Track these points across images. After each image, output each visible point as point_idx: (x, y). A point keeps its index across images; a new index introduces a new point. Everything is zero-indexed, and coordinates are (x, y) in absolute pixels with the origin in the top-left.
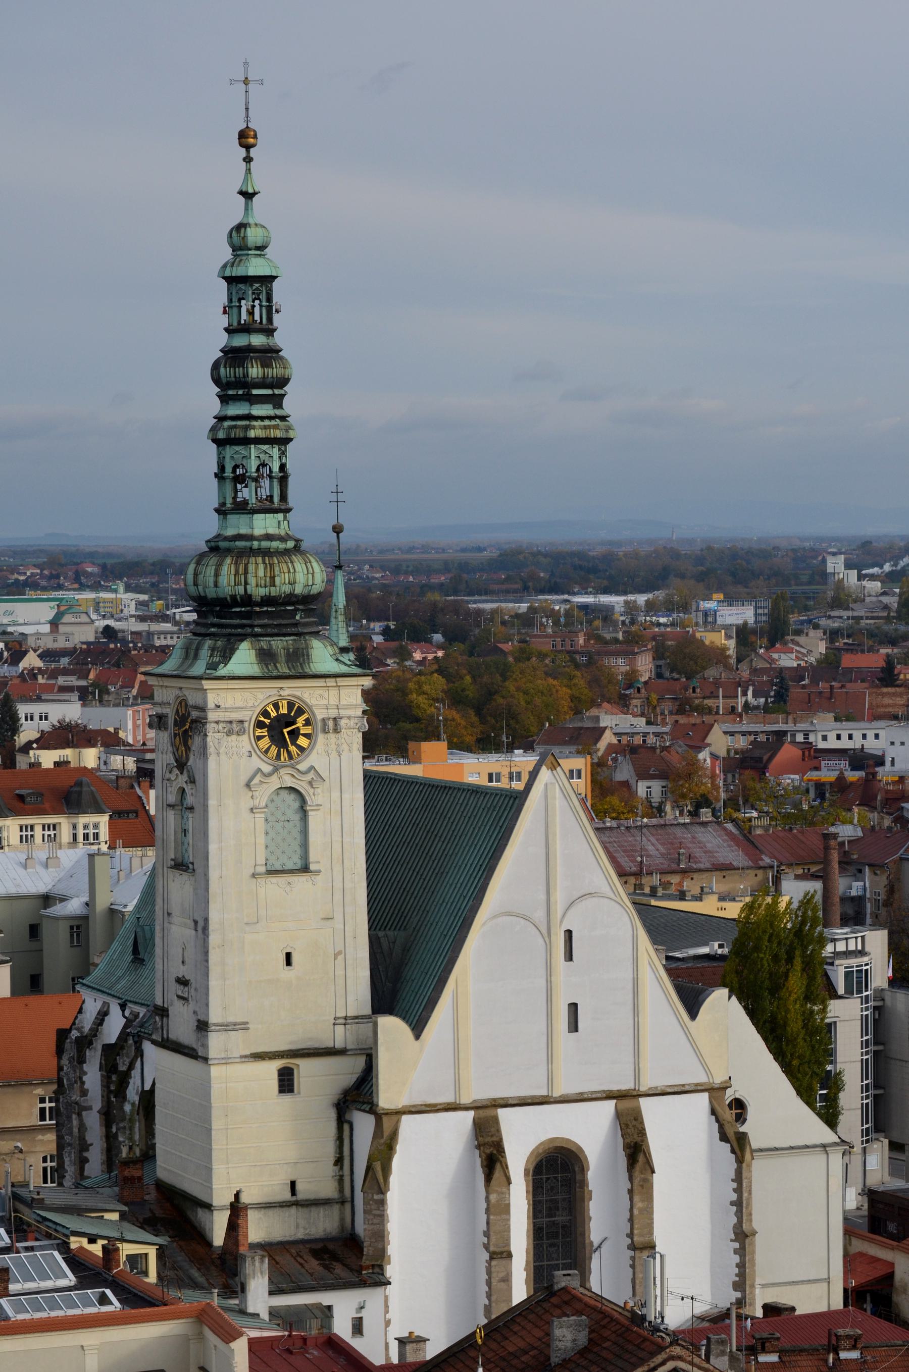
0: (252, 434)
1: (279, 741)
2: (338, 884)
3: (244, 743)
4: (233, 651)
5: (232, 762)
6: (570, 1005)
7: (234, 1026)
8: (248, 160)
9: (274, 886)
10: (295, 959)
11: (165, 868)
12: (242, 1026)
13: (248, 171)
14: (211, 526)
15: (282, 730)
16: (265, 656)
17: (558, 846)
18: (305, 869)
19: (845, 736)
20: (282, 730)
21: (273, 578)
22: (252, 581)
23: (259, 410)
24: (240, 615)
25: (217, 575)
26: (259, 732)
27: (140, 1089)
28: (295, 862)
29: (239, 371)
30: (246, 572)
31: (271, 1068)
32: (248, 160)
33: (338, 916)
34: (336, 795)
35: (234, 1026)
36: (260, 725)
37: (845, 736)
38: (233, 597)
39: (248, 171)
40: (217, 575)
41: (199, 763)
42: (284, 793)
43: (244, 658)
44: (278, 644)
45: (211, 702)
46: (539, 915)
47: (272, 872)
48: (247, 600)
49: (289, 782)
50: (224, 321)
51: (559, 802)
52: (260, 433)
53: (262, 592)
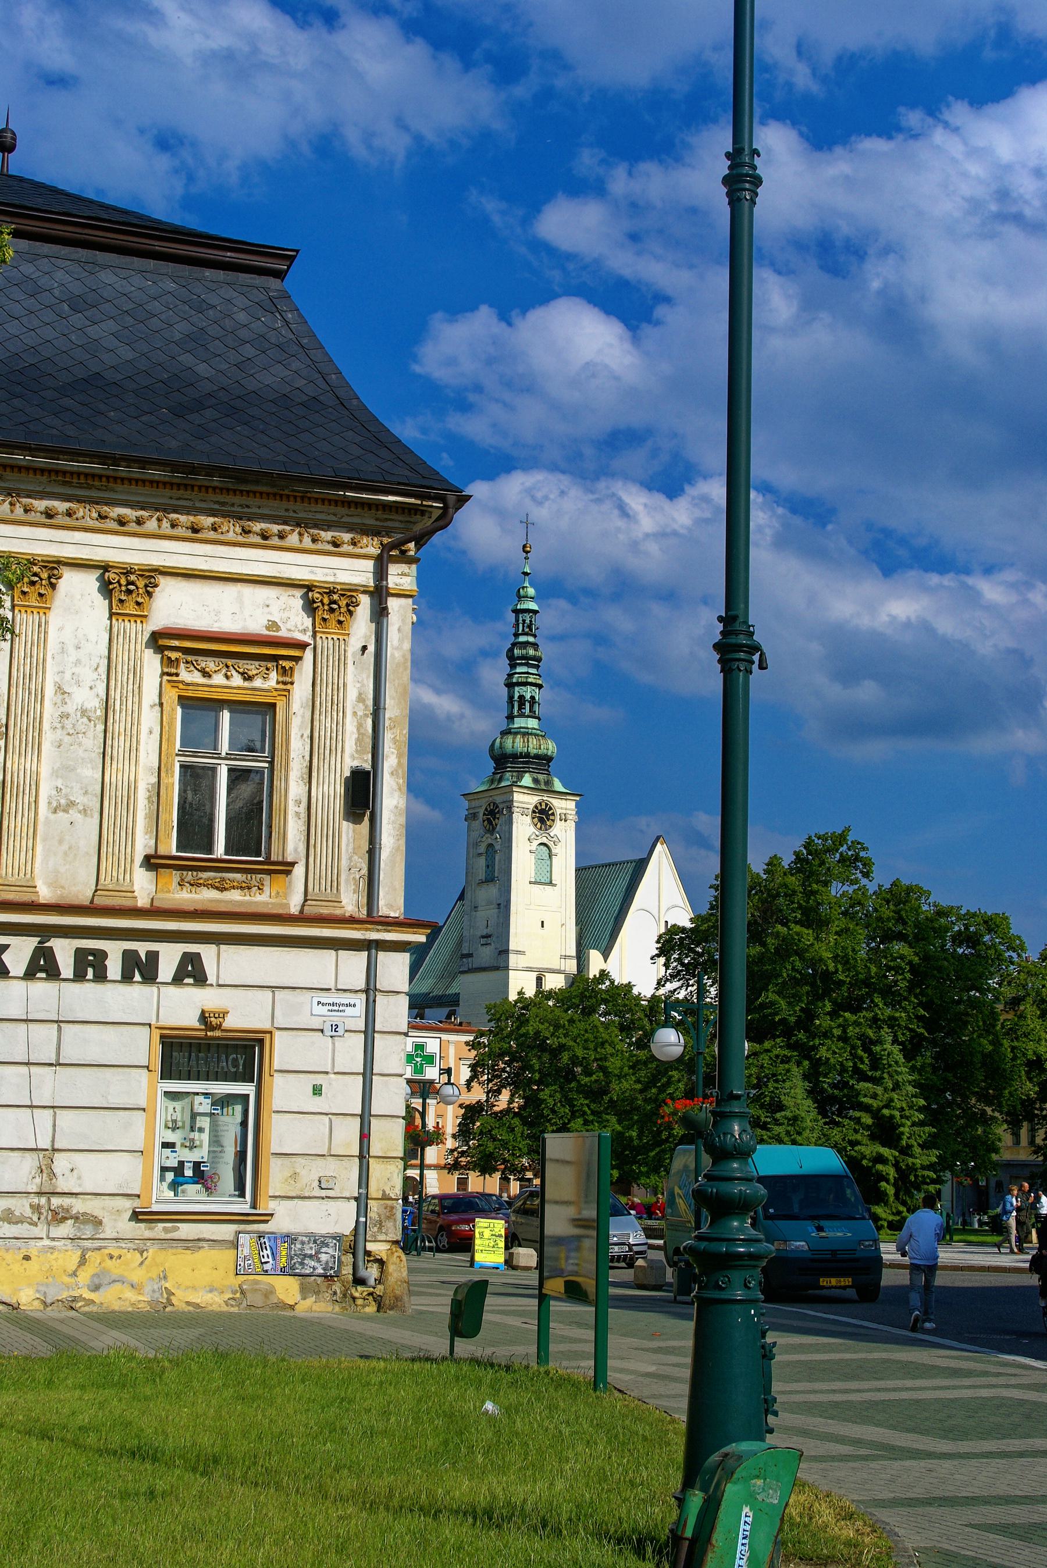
0: (530, 680)
1: (541, 820)
3: (528, 819)
4: (522, 777)
5: (523, 828)
6: (766, 668)
7: (518, 952)
11: (563, 840)
15: (543, 816)
16: (536, 781)
18: (550, 883)
19: (744, 1541)
20: (543, 816)
22: (531, 745)
23: (531, 671)
28: (548, 881)
29: (524, 652)
31: (534, 975)
35: (518, 952)
37: (744, 1541)
41: (505, 828)
43: (527, 780)
44: (541, 777)
45: (515, 799)
46: (655, 913)
47: (535, 883)
48: (527, 755)
49: (545, 840)
51: (664, 860)
52: (534, 681)
53: (535, 751)
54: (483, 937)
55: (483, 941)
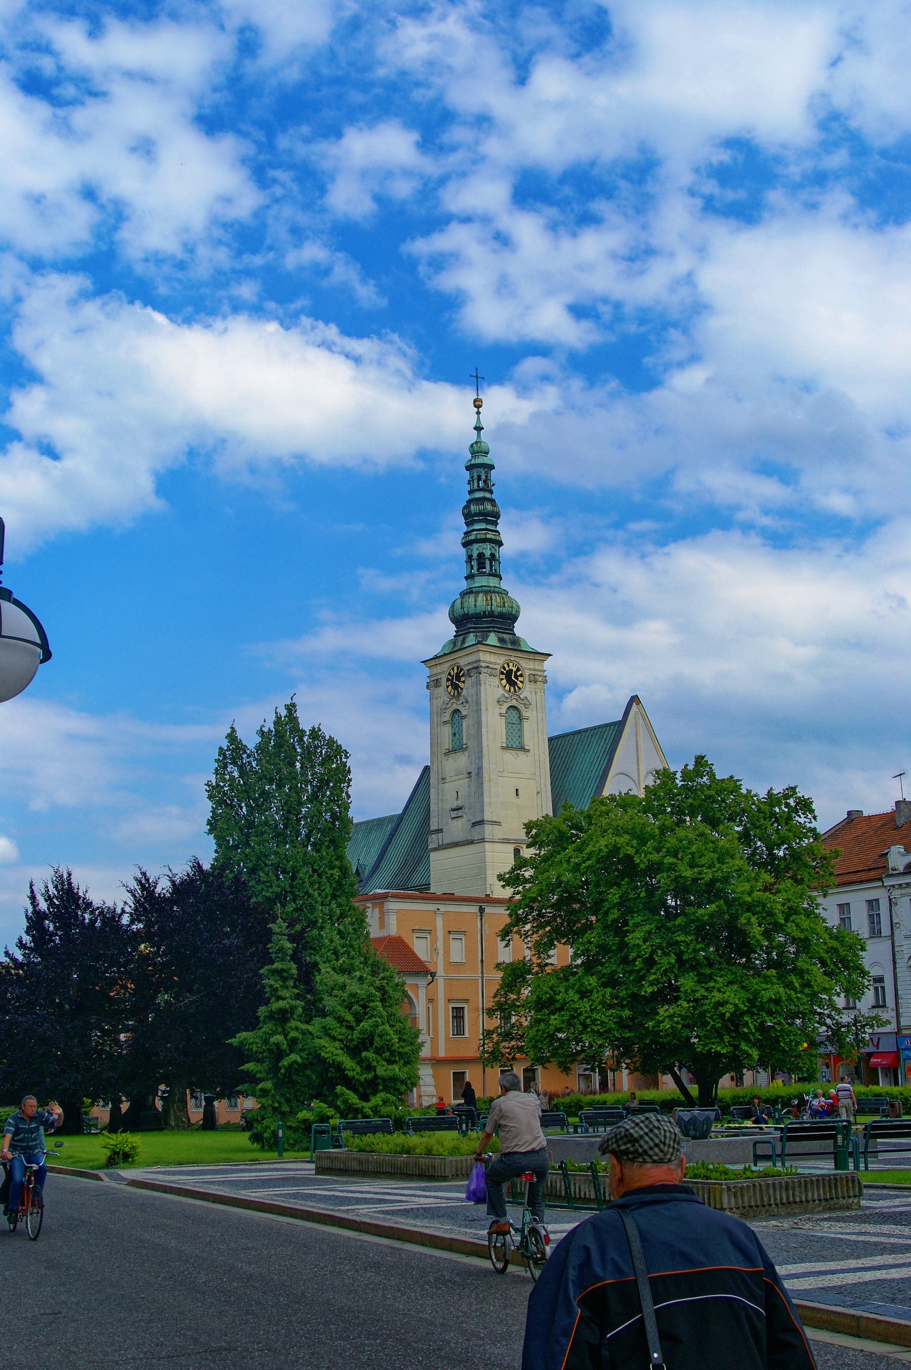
2: (537, 759)
3: (496, 681)
8: (478, 413)
9: (509, 756)
10: (520, 792)
12: (498, 823)
13: (479, 417)
14: (464, 585)
17: (641, 743)
21: (504, 603)
24: (486, 622)
25: (475, 601)
26: (502, 676)
27: (30, 909)
30: (491, 600)
32: (478, 413)
33: (538, 774)
34: (534, 713)
36: (502, 673)
38: (484, 612)
39: (479, 417)
40: (475, 601)
42: (511, 710)
50: (468, 488)
53: (499, 609)
54: (453, 810)
55: (454, 814)
